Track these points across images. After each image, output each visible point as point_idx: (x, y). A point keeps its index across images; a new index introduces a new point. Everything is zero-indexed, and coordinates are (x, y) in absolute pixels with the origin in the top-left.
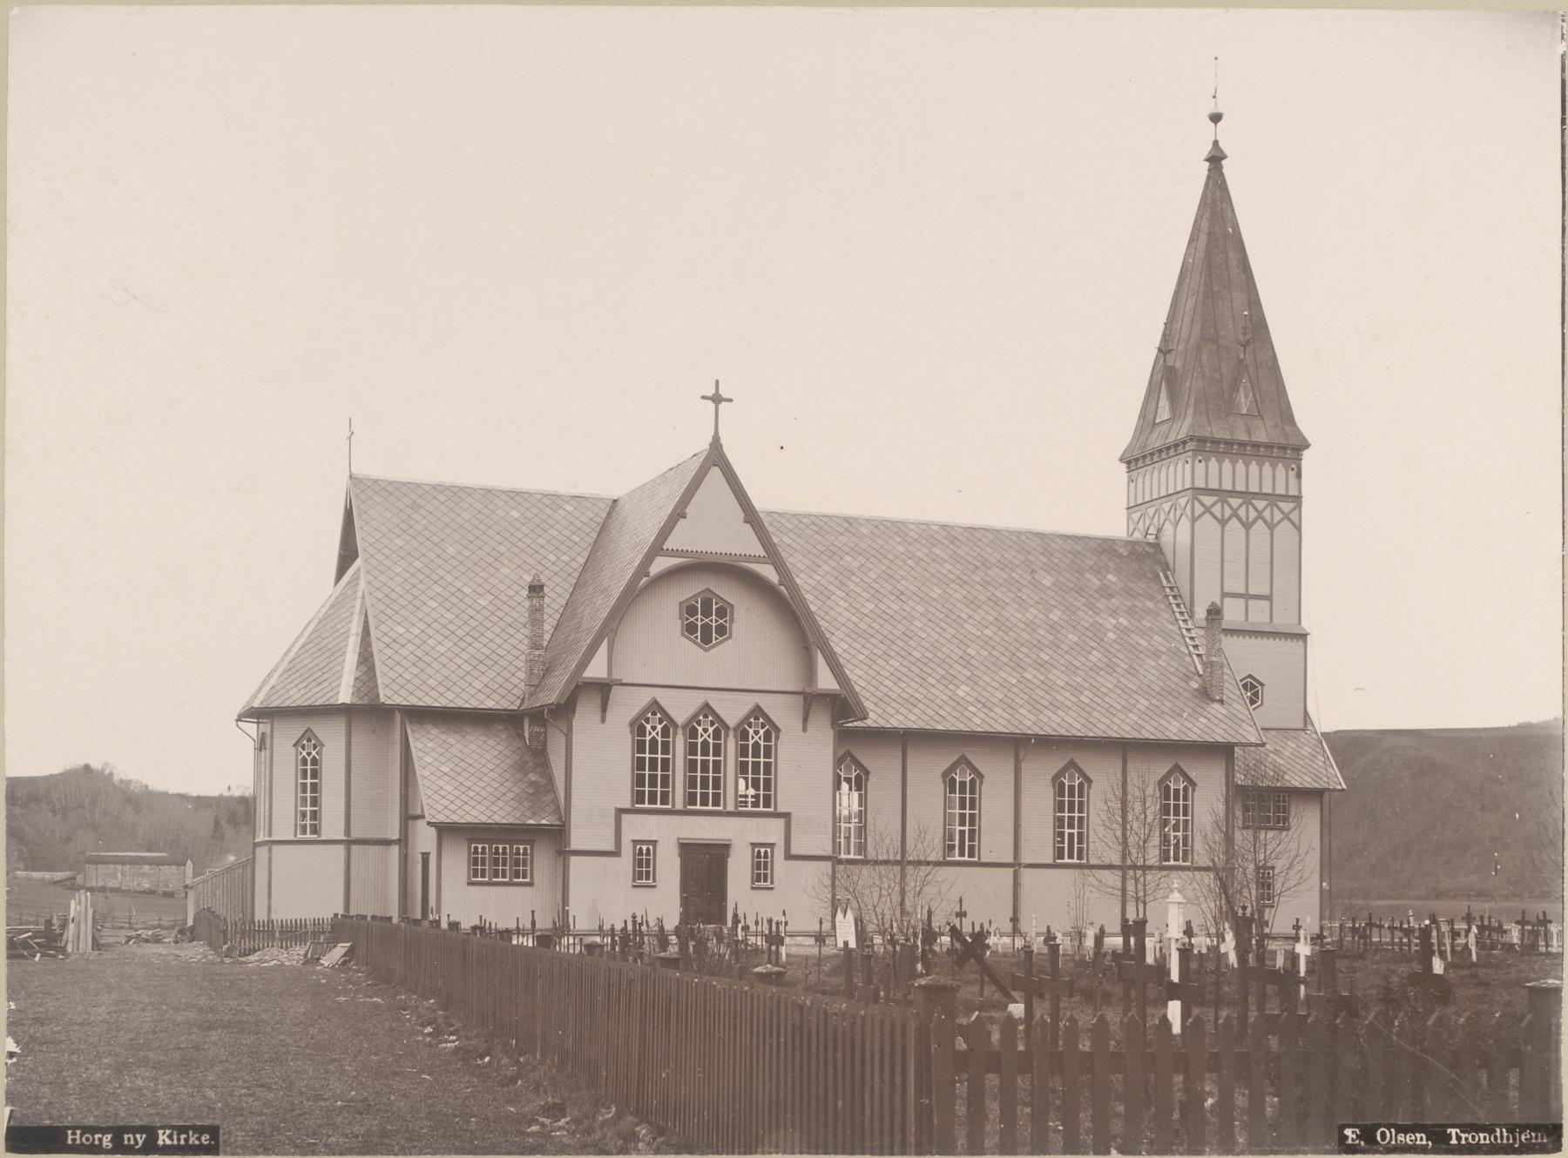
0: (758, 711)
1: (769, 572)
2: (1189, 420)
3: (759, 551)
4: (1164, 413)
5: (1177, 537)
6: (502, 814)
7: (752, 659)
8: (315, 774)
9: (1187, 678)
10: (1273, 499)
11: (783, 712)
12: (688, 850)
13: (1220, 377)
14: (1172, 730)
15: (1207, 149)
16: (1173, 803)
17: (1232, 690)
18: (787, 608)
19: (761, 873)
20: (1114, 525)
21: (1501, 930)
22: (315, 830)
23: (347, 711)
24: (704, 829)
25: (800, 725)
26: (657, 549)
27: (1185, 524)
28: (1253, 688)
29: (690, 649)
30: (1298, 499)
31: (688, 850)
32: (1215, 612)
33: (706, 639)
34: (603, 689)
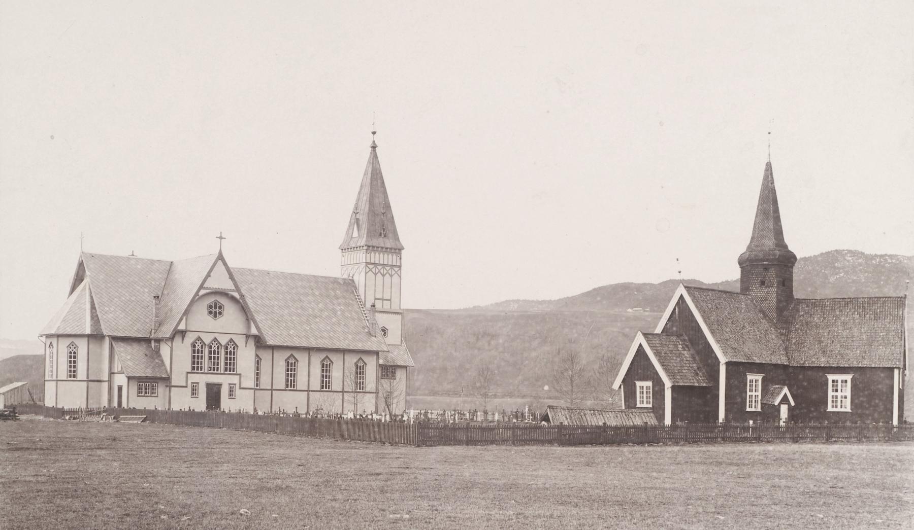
0: (231, 340)
1: (236, 295)
2: (365, 239)
3: (233, 288)
4: (355, 234)
5: (359, 279)
6: (149, 373)
7: (230, 323)
8: (75, 357)
9: (364, 328)
10: (392, 266)
11: (240, 341)
12: (209, 386)
13: (377, 225)
14: (360, 346)
15: (370, 143)
16: (360, 371)
17: (380, 333)
18: (244, 309)
19: (231, 393)
20: (337, 272)
21: (464, 415)
22: (74, 376)
23: (89, 336)
24: (214, 379)
25: (68, 289)
26: (201, 287)
27: (363, 274)
28: (384, 331)
29: (210, 318)
30: (400, 267)
31: (209, 386)
32: (373, 306)
33: (215, 316)
34: (183, 333)
